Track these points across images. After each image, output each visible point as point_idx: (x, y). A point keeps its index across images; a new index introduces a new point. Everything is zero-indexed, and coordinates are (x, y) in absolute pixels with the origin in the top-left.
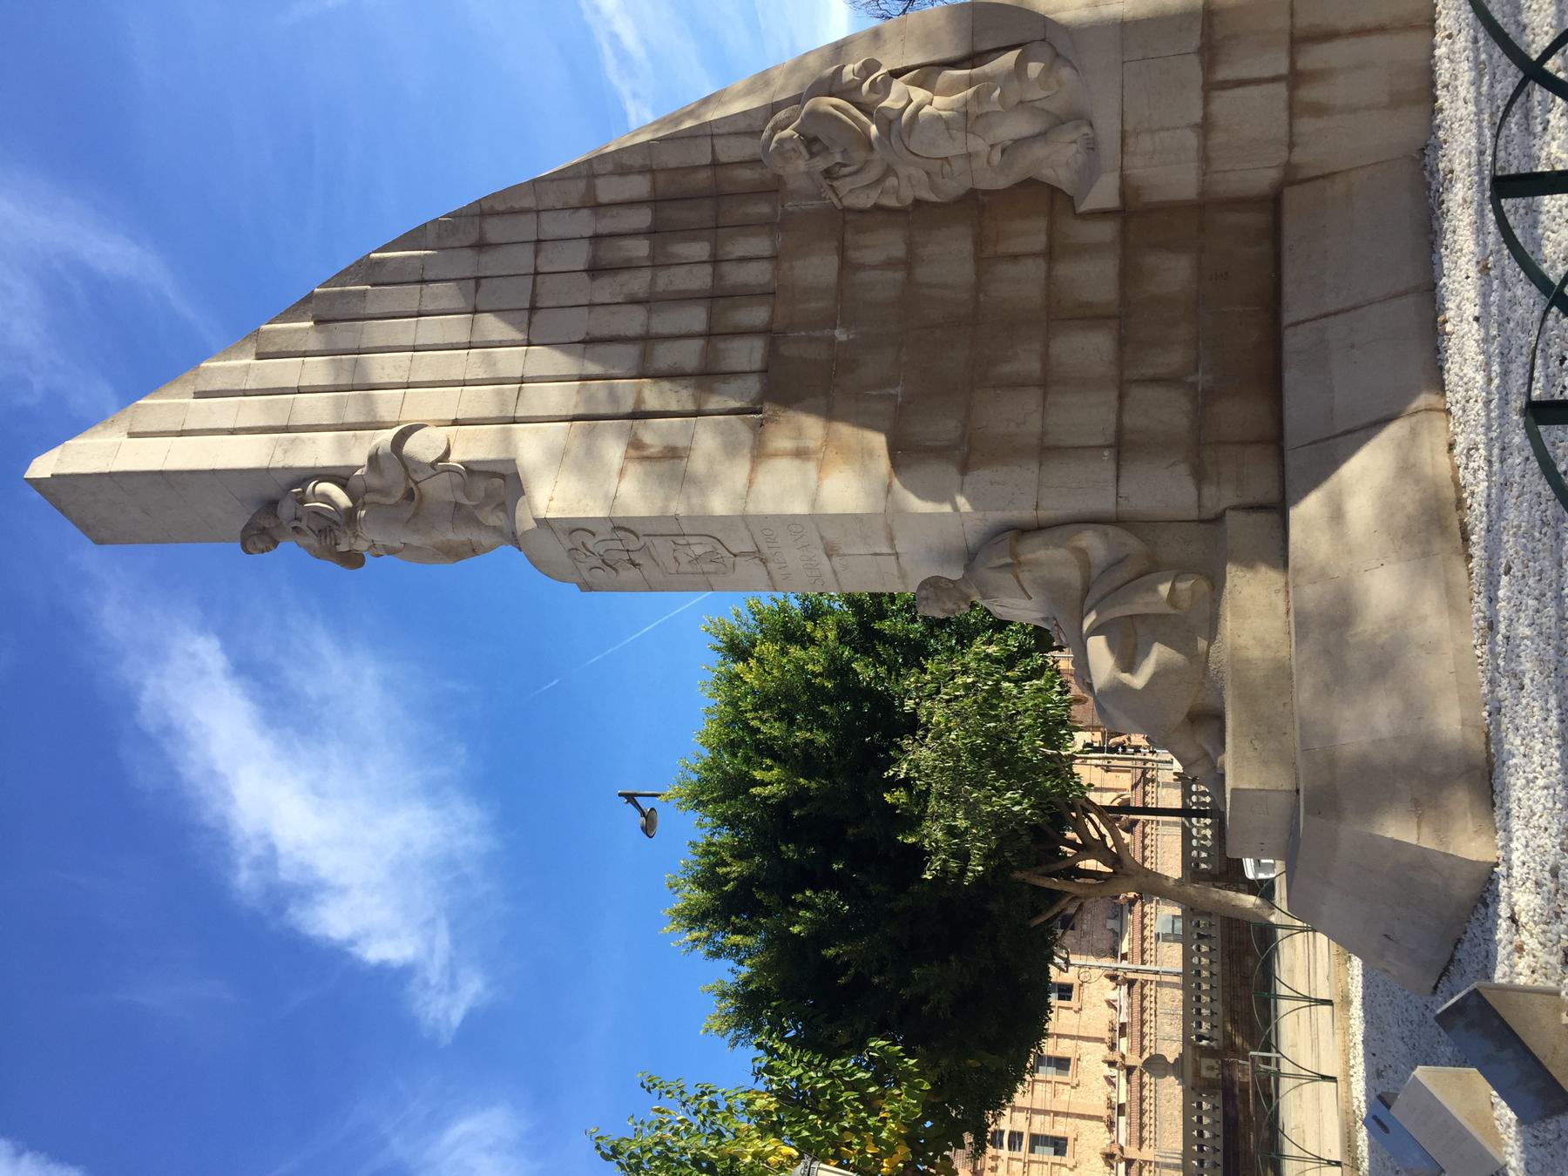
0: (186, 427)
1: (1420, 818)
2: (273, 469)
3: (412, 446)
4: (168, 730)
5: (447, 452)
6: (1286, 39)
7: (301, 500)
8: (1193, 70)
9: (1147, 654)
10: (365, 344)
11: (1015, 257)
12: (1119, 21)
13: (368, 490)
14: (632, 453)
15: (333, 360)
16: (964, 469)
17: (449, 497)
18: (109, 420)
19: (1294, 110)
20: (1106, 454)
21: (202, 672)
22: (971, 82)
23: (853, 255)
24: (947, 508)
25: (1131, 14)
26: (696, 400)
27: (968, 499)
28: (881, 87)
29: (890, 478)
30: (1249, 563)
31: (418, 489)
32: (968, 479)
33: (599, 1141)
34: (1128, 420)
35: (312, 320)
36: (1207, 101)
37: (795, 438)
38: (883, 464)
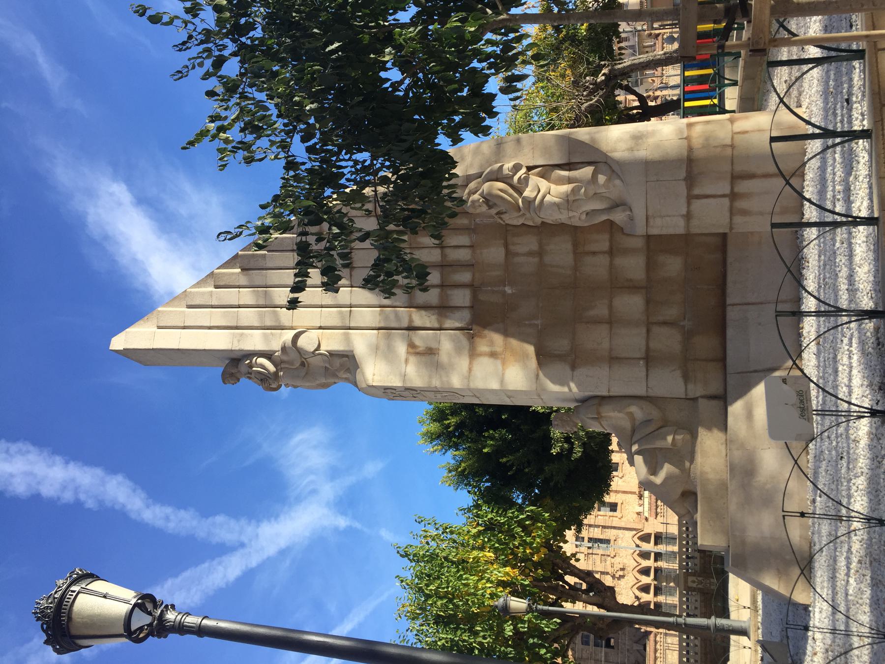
0: (186, 324)
1: (780, 578)
2: (234, 350)
3: (302, 342)
4: (106, 237)
5: (319, 346)
6: (729, 176)
7: (251, 366)
8: (682, 188)
9: (662, 468)
10: (270, 283)
11: (594, 253)
12: (644, 161)
13: (282, 362)
14: (411, 350)
15: (254, 291)
16: (573, 367)
17: (322, 364)
18: (146, 318)
19: (732, 212)
20: (641, 362)
21: (120, 204)
22: (570, 181)
23: (511, 248)
24: (566, 389)
25: (650, 157)
26: (439, 321)
27: (575, 384)
28: (523, 181)
29: (538, 371)
30: (709, 428)
31: (307, 361)
32: (575, 373)
33: (399, 549)
34: (651, 345)
35: (240, 268)
36: (689, 204)
37: (490, 346)
38: (533, 362)
